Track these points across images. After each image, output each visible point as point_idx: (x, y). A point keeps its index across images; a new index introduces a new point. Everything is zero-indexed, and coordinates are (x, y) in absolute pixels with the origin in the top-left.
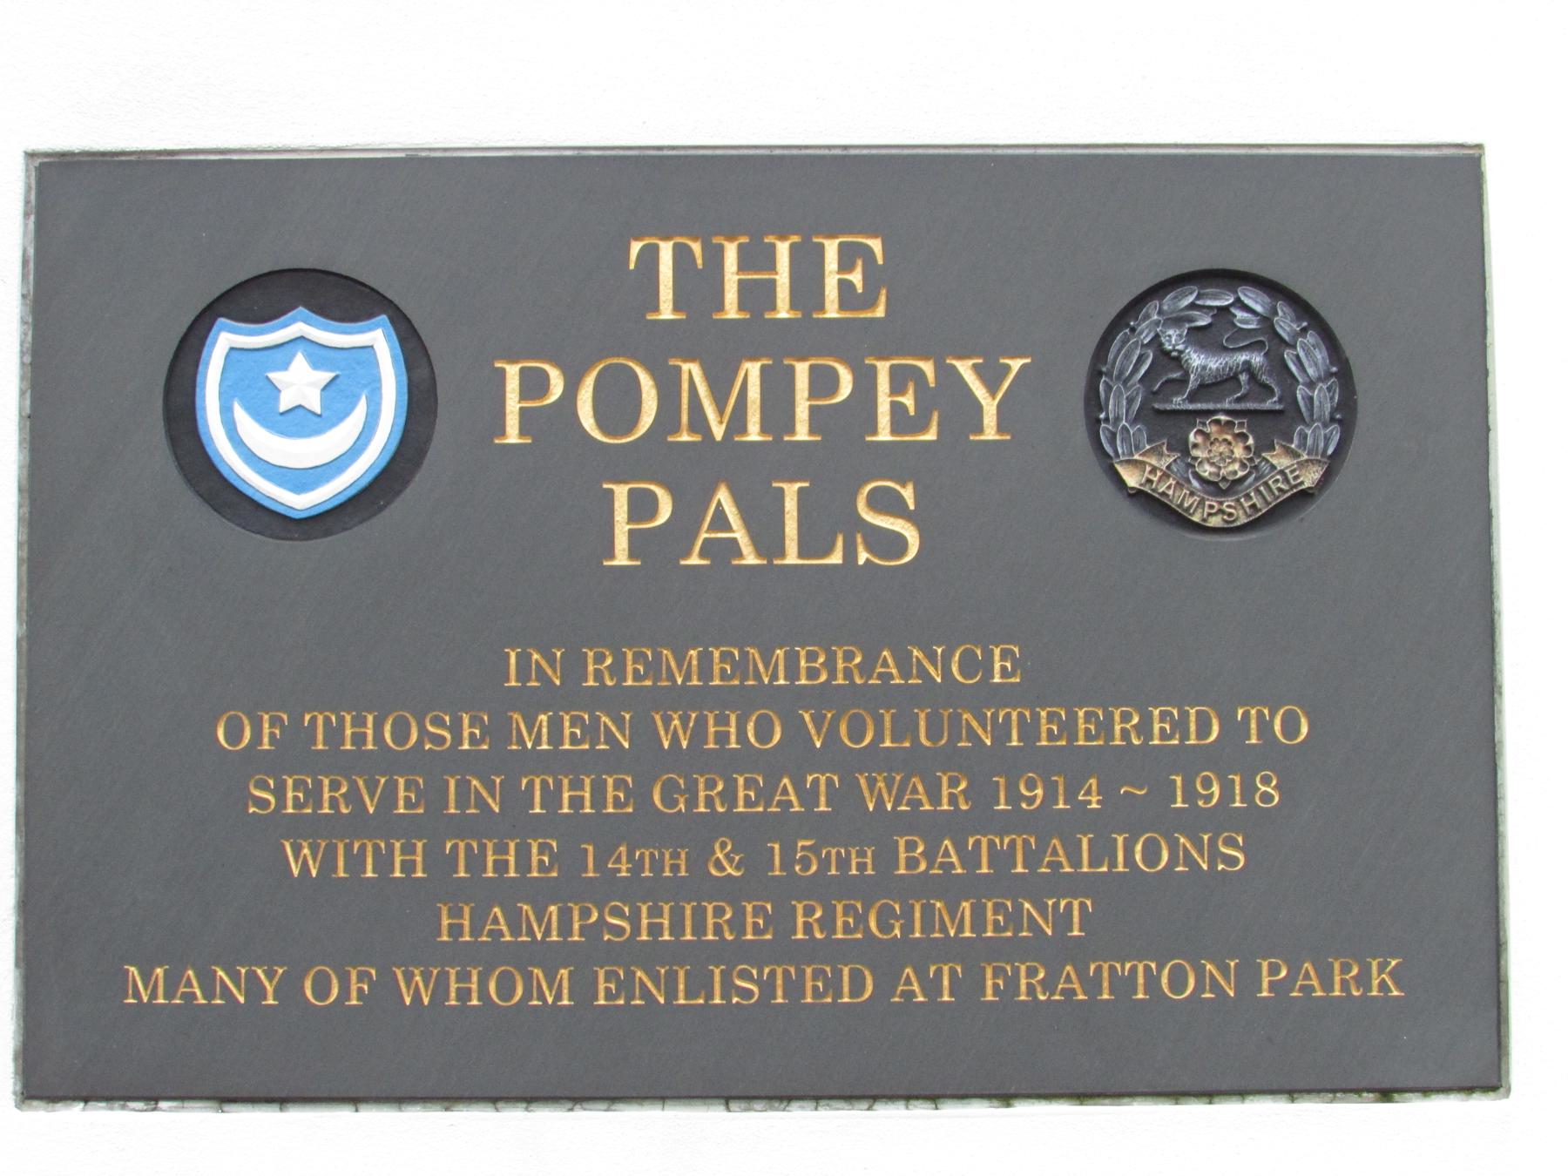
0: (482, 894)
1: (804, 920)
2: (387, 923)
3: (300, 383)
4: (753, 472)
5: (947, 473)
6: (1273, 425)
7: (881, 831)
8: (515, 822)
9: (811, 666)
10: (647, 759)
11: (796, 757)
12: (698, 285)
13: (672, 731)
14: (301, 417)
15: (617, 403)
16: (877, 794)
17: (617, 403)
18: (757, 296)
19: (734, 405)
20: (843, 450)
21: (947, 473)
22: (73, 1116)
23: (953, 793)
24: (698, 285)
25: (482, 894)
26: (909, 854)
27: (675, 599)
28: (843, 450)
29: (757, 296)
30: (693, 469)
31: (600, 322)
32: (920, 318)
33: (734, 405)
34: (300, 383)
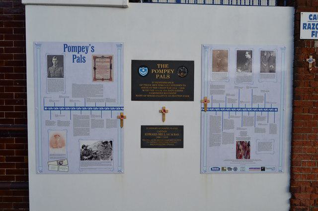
0: (151, 92)
1: (169, 90)
2: (147, 93)
3: (143, 70)
4: (162, 74)
5: (171, 74)
6: (185, 73)
7: (167, 89)
8: (152, 89)
9: (165, 82)
10: (158, 86)
11: (164, 86)
12: (160, 66)
13: (159, 85)
14: (143, 72)
15: (157, 71)
16: (167, 88)
17: (157, 71)
18: (163, 67)
19: (161, 71)
20: (166, 73)
21: (171, 74)
22: (30, 208)
23: (171, 88)
24: (160, 66)
25: (151, 92)
26: (169, 90)
27: (159, 80)
28: (166, 73)
29: (163, 67)
30: (160, 74)
31: (156, 68)
32: (170, 68)
33: (161, 71)
34: (143, 70)
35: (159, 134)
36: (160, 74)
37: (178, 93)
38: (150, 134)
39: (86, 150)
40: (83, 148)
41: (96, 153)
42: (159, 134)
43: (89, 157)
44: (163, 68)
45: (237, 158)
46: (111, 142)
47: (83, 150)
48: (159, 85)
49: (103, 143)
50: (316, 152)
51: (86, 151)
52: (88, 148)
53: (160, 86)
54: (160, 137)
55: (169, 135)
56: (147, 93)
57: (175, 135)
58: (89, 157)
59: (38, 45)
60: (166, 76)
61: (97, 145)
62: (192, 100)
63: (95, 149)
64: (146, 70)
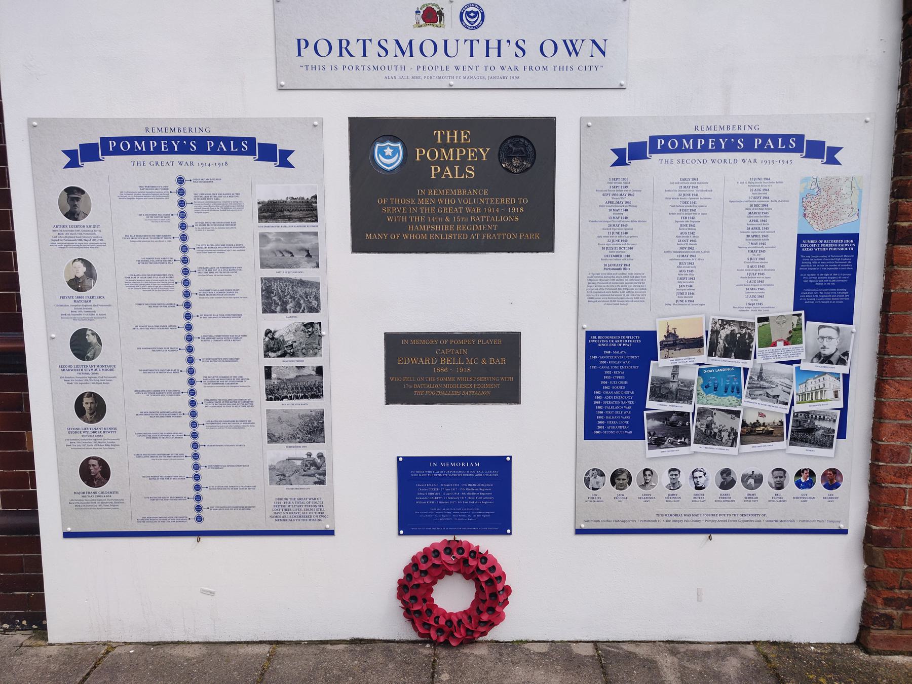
0: (415, 224)
2: (402, 228)
3: (389, 152)
4: (452, 165)
5: (478, 165)
7: (468, 215)
10: (437, 205)
11: (457, 205)
12: (444, 137)
13: (440, 201)
15: (433, 155)
16: (468, 210)
17: (433, 155)
18: (452, 139)
19: (448, 155)
20: (464, 161)
21: (478, 165)
24: (444, 137)
25: (415, 224)
27: (442, 182)
29: (452, 139)
31: (430, 143)
32: (475, 142)
33: (448, 155)
34: (389, 152)
35: (443, 360)
36: (443, 164)
37: (502, 227)
38: (414, 361)
39: (273, 339)
40: (266, 335)
41: (292, 345)
42: (443, 360)
43: (279, 353)
44: (452, 145)
45: (589, 334)
46: (320, 323)
47: (267, 339)
48: (440, 201)
49: (305, 325)
50: (799, 315)
51: (272, 342)
52: (276, 336)
53: (444, 205)
54: (445, 370)
55: (472, 361)
56: (402, 228)
57: (492, 361)
58: (279, 353)
59: (35, 127)
60: (462, 171)
61: (293, 329)
62: (550, 248)
63: (289, 338)
64: (396, 151)
